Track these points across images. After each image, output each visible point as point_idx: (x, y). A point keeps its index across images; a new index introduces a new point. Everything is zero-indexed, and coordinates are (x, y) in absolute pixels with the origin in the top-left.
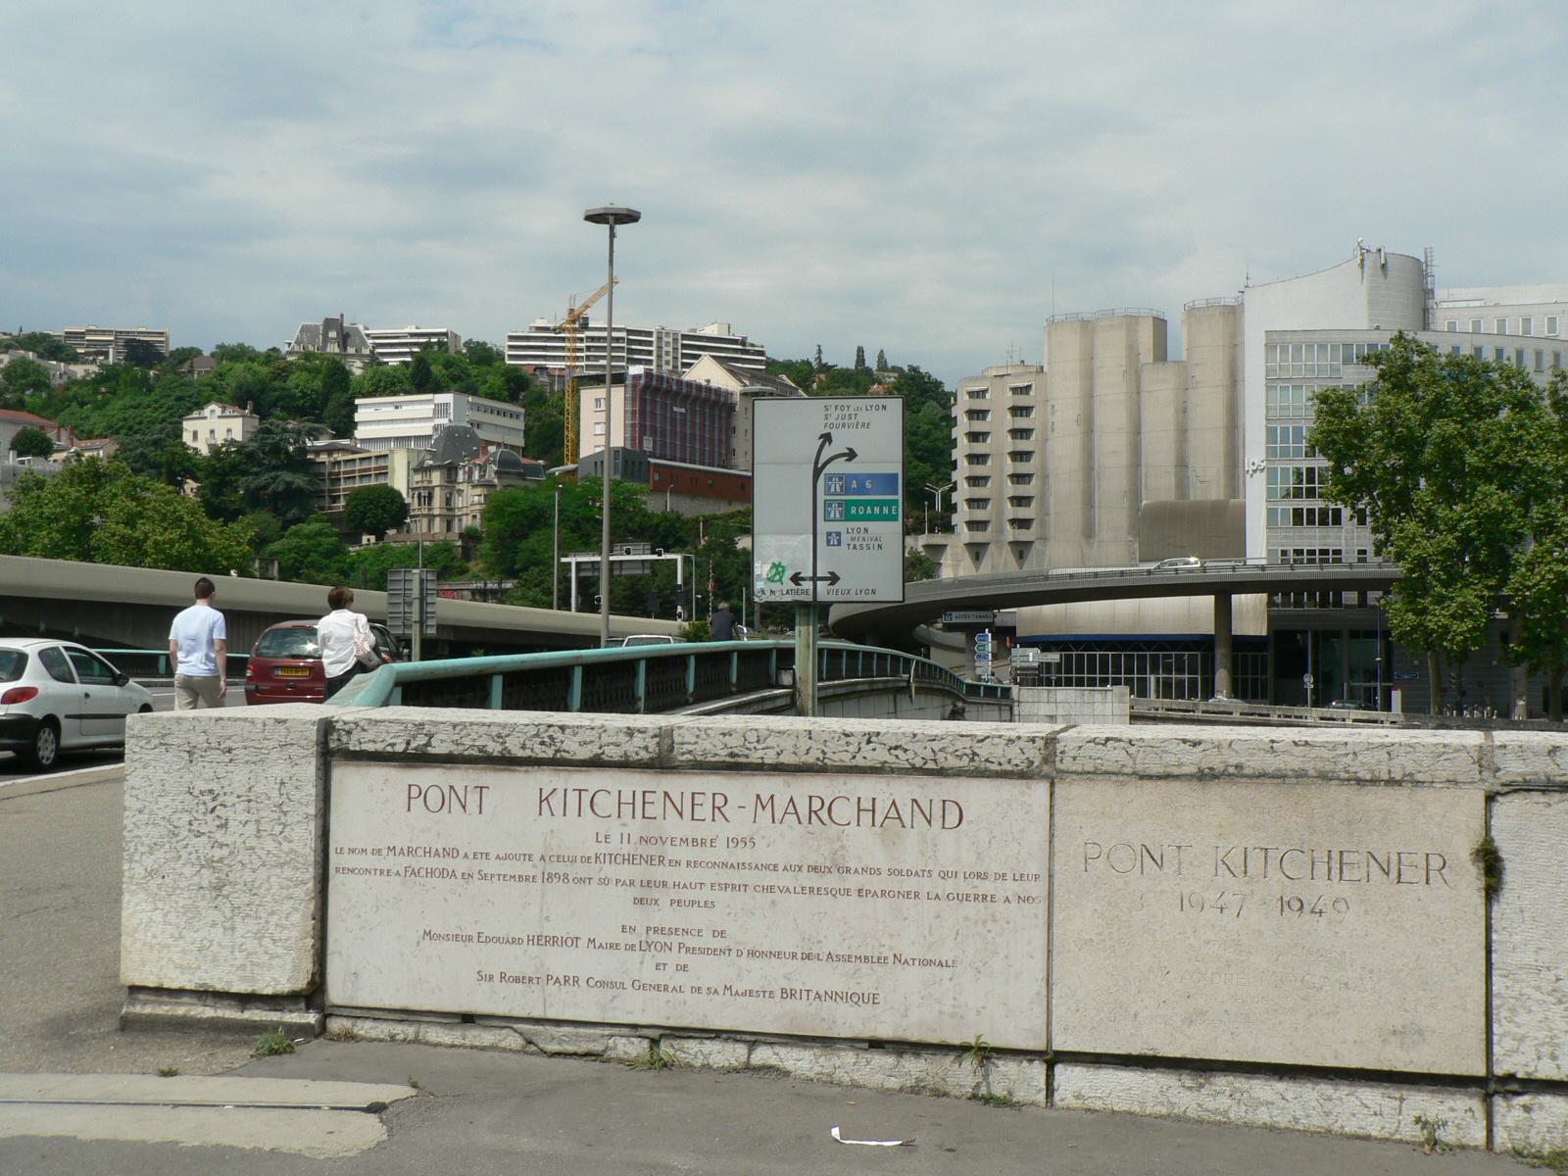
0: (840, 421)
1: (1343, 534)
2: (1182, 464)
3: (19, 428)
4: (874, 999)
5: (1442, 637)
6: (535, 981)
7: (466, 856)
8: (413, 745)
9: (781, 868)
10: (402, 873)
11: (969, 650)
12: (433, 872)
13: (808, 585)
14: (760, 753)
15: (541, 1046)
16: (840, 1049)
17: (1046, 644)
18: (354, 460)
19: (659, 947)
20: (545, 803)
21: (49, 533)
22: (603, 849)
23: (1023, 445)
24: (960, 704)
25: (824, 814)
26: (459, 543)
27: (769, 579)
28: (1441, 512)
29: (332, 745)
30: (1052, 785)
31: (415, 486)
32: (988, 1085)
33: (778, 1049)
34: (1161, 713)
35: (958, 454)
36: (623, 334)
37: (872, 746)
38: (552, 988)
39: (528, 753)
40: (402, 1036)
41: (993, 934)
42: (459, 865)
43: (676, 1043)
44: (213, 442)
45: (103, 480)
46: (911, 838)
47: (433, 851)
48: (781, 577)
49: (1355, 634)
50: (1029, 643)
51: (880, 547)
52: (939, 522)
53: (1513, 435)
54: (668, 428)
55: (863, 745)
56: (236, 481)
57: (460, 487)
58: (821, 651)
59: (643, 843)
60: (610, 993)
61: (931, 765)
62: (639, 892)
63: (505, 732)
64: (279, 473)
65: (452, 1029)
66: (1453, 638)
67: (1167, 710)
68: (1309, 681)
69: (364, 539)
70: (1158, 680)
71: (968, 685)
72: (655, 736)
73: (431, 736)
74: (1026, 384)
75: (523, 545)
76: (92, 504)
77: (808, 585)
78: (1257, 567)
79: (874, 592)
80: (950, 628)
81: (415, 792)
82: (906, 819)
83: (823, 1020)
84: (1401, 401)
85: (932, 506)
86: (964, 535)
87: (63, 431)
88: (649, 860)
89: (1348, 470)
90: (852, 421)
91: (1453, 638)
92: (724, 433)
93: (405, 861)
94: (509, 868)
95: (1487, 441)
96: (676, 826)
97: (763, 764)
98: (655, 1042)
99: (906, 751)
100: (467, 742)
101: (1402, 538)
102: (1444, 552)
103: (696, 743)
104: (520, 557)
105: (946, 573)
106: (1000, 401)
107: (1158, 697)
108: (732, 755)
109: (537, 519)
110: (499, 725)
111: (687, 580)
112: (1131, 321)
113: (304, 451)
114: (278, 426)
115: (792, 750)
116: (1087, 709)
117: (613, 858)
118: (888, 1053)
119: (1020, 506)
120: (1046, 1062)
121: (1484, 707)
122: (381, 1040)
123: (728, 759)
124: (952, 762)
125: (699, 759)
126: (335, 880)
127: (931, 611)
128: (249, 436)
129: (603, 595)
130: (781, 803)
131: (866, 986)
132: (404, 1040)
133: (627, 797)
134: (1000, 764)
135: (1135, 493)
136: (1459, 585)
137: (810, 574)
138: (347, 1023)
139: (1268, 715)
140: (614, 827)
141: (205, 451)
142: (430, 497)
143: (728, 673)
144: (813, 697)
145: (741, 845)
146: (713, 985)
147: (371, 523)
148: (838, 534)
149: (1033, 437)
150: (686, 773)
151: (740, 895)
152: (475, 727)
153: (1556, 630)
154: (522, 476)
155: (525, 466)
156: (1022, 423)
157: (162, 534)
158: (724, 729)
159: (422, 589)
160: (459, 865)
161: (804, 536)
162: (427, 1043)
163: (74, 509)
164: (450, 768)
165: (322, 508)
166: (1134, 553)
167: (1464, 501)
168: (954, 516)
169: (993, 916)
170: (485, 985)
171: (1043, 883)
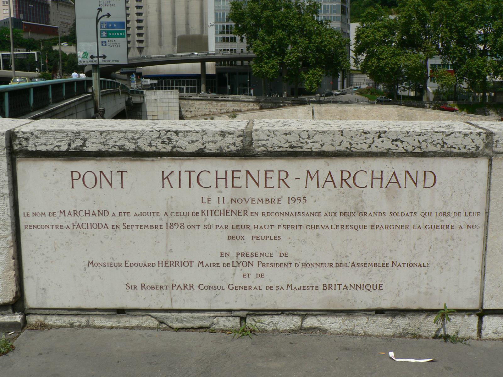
0: (104, 4)
1: (237, 44)
2: (187, 24)
4: (380, 288)
5: (267, 74)
6: (165, 288)
7: (114, 214)
8: (73, 146)
9: (323, 214)
10: (71, 226)
11: (129, 80)
12: (92, 226)
13: (96, 59)
14: (310, 145)
15: (170, 324)
16: (358, 316)
17: (152, 77)
19: (245, 264)
20: (166, 181)
22: (206, 207)
23: (140, 18)
25: (350, 181)
27: (83, 57)
28: (266, 38)
29: (16, 148)
30: (491, 160)
32: (445, 329)
33: (319, 318)
34: (187, 97)
37: (381, 139)
38: (176, 291)
39: (154, 149)
40: (78, 324)
41: (451, 247)
42: (110, 221)
43: (256, 318)
46: (405, 193)
47: (91, 213)
48: (87, 57)
49: (240, 74)
50: (147, 77)
51: (120, 46)
53: (286, 15)
54: (28, 11)
55: (376, 139)
58: (101, 81)
59: (233, 202)
60: (214, 292)
61: (417, 150)
62: (230, 232)
63: (137, 136)
65: (110, 318)
66: (270, 74)
68: (229, 87)
72: (240, 136)
73: (85, 140)
77: (96, 59)
78: (213, 54)
79: (118, 61)
80: (122, 73)
81: (76, 176)
82: (402, 182)
83: (348, 300)
84: (255, 5)
88: (238, 213)
89: (240, 25)
90: (109, 4)
91: (270, 74)
92: (252, 208)
93: (72, 219)
94: (144, 221)
95: (278, 17)
96: (253, 191)
97: (312, 152)
98: (243, 319)
99: (402, 142)
100: (111, 143)
101: (255, 45)
102: (267, 49)
103: (268, 140)
108: (291, 147)
110: (133, 132)
111: (39, 59)
115: (330, 143)
116: (166, 97)
117: (213, 212)
118: (387, 316)
119: (140, 36)
120: (478, 315)
121: (275, 94)
122: (64, 327)
123: (289, 149)
124: (431, 148)
125: (269, 149)
126: (24, 233)
130: (323, 176)
131: (375, 280)
132: (79, 326)
133: (221, 175)
134: (459, 149)
135: (174, 33)
136: (271, 59)
137: (96, 55)
138: (41, 318)
139: (218, 97)
140: (214, 194)
143: (74, 89)
145: (297, 201)
146: (280, 285)
148: (105, 42)
149: (143, 15)
150: (260, 159)
151: (296, 232)
152: (116, 133)
153: (297, 72)
156: (140, 11)
158: (286, 130)
160: (110, 221)
162: (95, 327)
164: (100, 160)
167: (273, 35)
169: (452, 237)
170: (132, 292)
171: (482, 218)
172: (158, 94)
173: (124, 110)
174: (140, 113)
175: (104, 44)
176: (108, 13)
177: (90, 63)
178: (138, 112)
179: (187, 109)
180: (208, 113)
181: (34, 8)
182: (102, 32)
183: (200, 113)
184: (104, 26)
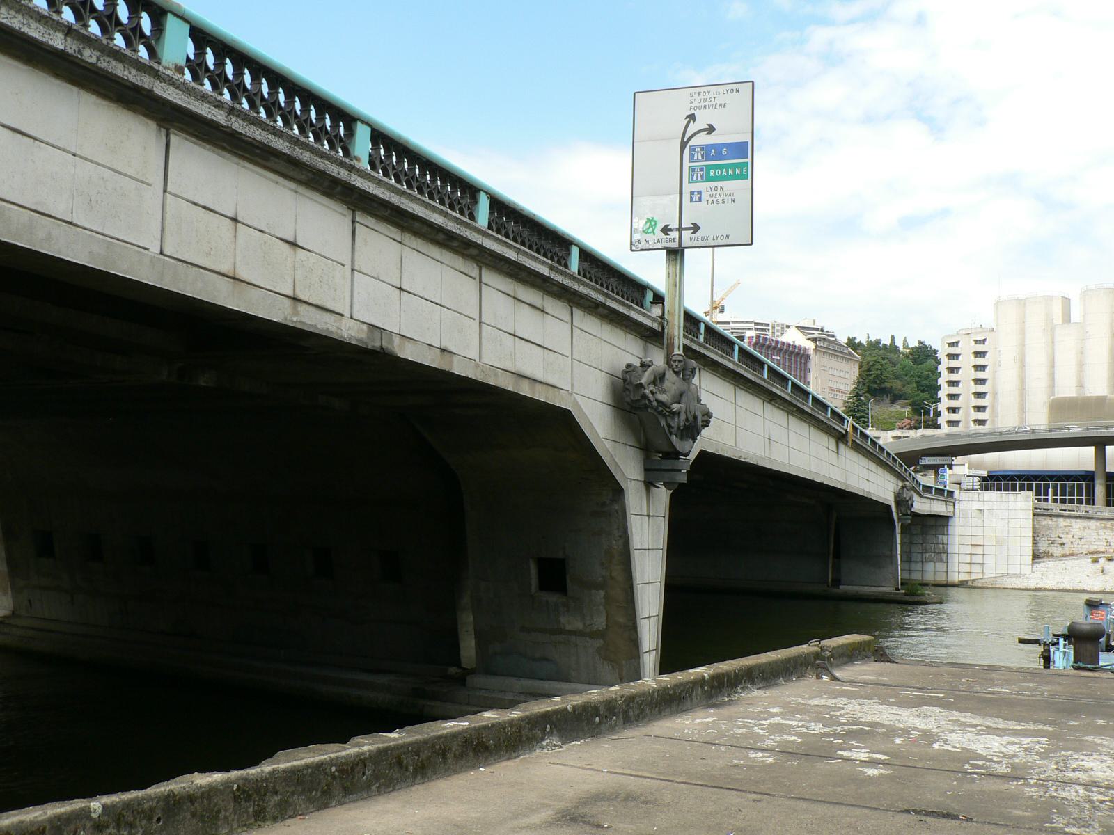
0: (703, 104)
13: (674, 235)
27: (644, 231)
34: (1054, 512)
35: (942, 381)
36: (752, 325)
48: (653, 230)
51: (733, 201)
67: (1061, 510)
74: (983, 338)
90: (712, 102)
92: (803, 372)
106: (966, 349)
112: (1048, 299)
119: (979, 411)
148: (700, 192)
149: (987, 369)
161: (672, 196)
168: (939, 419)
172: (985, 500)
174: (945, 538)
175: (696, 197)
176: (709, 125)
177: (660, 245)
178: (940, 537)
179: (1054, 537)
180: (1103, 550)
181: (781, 361)
182: (693, 170)
183: (1083, 547)
184: (698, 154)
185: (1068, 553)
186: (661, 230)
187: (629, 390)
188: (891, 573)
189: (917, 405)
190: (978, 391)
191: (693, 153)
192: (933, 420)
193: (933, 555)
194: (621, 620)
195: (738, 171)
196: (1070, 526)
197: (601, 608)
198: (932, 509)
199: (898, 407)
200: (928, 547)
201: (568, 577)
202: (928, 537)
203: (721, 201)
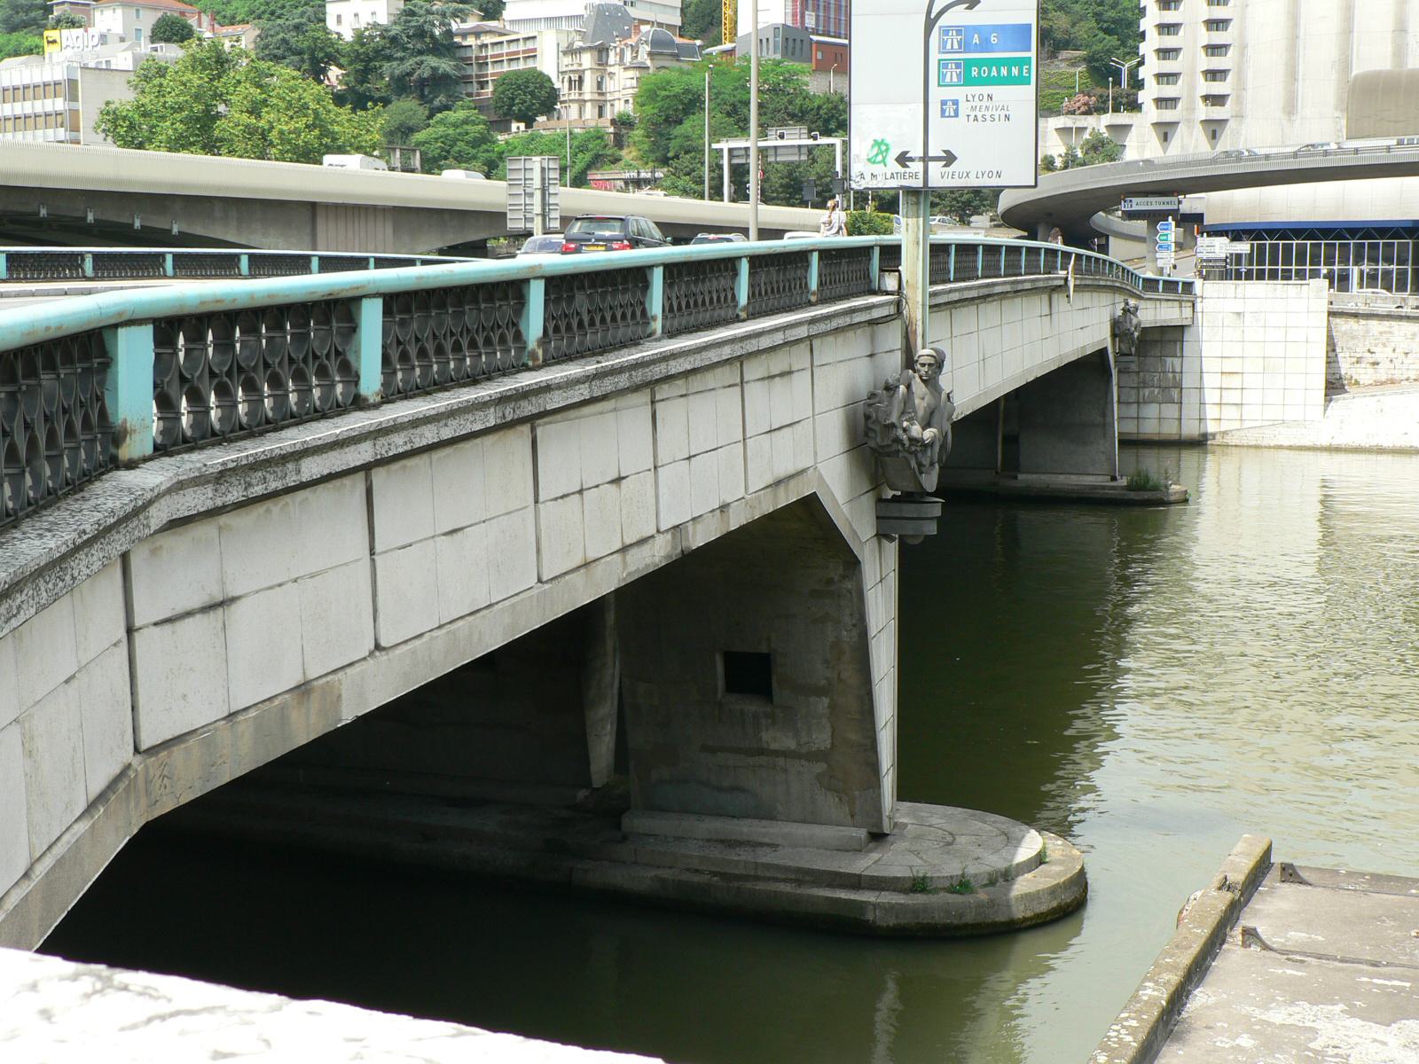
3: (159, 14)
11: (1149, 239)
13: (917, 167)
17: (1236, 234)
18: (502, 43)
21: (173, 124)
24: (1132, 302)
26: (611, 130)
27: (869, 160)
31: (565, 69)
44: (358, 26)
45: (226, 66)
48: (884, 158)
50: (1216, 232)
51: (1007, 118)
52: (1124, 100)
56: (381, 67)
57: (610, 69)
64: (424, 58)
69: (514, 126)
70: (1362, 272)
71: (1145, 280)
75: (678, 130)
76: (215, 91)
80: (1131, 215)
85: (1117, 82)
86: (1150, 113)
87: (204, 17)
104: (674, 144)
105: (1130, 154)
107: (1361, 287)
109: (691, 103)
113: (449, 34)
114: (422, 7)
119: (1214, 79)
127: (1109, 198)
128: (392, 18)
129: (753, 188)
135: (1345, 63)
141: (348, 36)
142: (581, 80)
144: (923, 305)
147: (520, 110)
148: (956, 102)
154: (676, 57)
155: (678, 46)
157: (287, 123)
159: (543, 179)
163: (197, 97)
165: (469, 95)
166: (1340, 131)
168: (1140, 93)
173: (1103, 352)
174: (1177, 361)
175: (950, 110)
178: (1169, 360)
179: (1361, 351)
182: (946, 66)
184: (953, 41)
185: (1383, 379)
186: (897, 160)
187: (875, 431)
188: (1103, 453)
189: (1097, 60)
190: (1212, 43)
191: (945, 38)
192: (1128, 95)
193: (1156, 391)
194: (853, 736)
195: (1015, 71)
196: (1390, 333)
197: (824, 720)
198: (1158, 318)
199: (1063, 65)
200: (1148, 376)
201: (774, 679)
202: (1149, 361)
203: (988, 118)
